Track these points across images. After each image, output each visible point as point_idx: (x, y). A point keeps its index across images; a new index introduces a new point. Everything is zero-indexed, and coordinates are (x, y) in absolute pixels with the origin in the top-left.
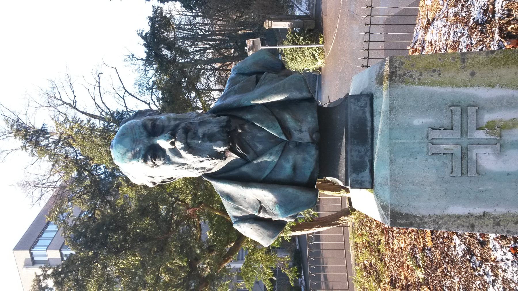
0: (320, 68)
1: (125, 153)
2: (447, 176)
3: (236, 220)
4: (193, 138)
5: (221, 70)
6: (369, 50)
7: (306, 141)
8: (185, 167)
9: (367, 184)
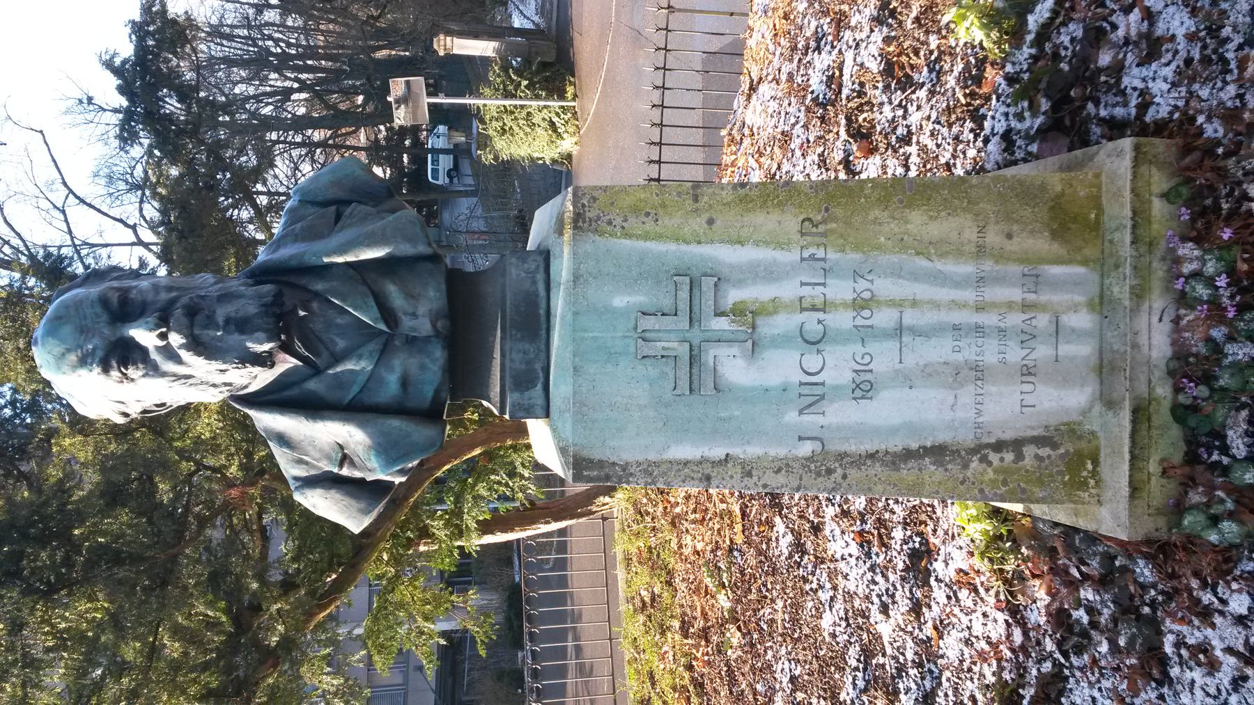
0: (569, 157)
1: (63, 354)
2: (668, 395)
3: (298, 484)
4: (206, 327)
5: (331, 146)
6: (661, 125)
7: (424, 333)
8: (200, 382)
9: (539, 411)
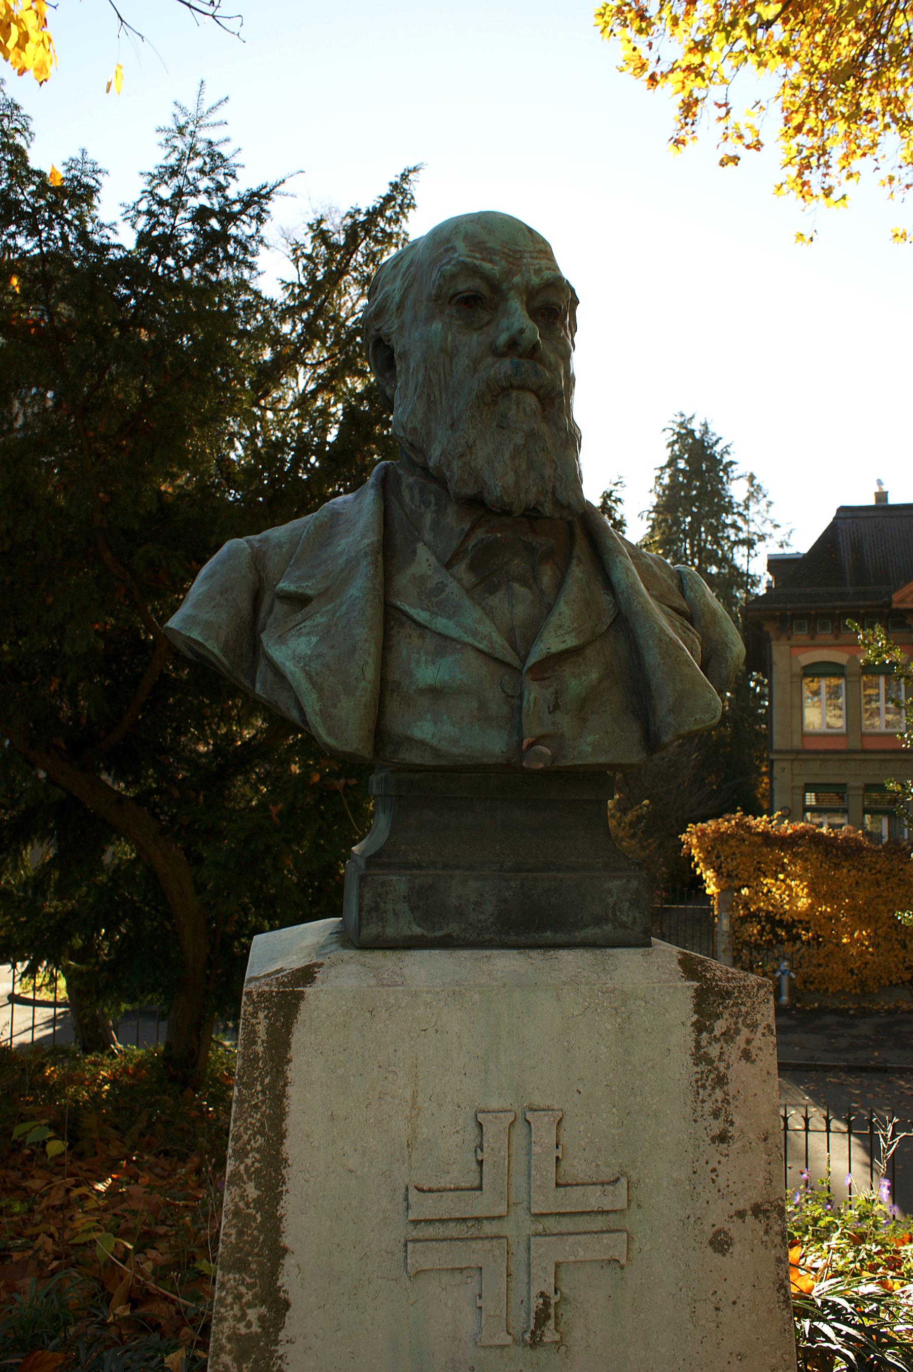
1: (266, 246)
